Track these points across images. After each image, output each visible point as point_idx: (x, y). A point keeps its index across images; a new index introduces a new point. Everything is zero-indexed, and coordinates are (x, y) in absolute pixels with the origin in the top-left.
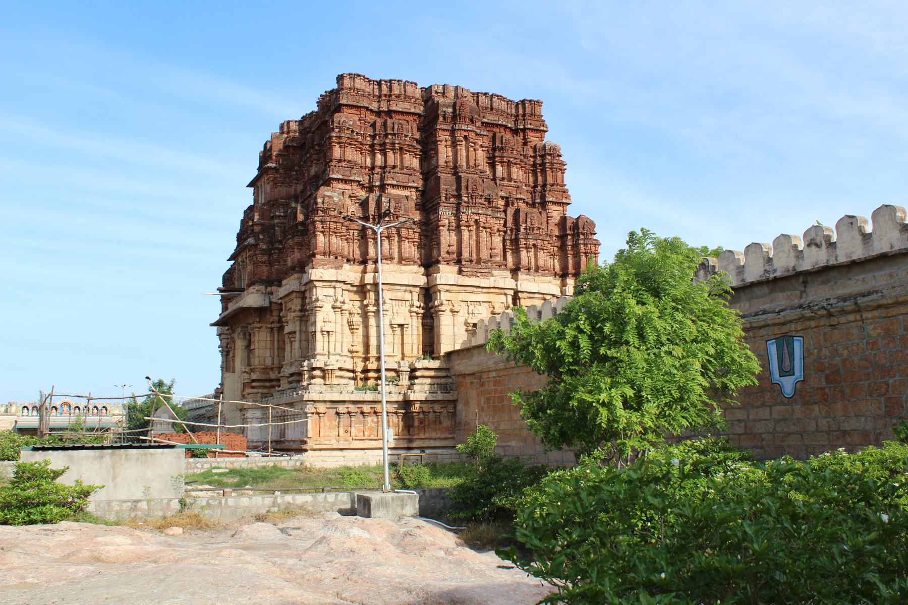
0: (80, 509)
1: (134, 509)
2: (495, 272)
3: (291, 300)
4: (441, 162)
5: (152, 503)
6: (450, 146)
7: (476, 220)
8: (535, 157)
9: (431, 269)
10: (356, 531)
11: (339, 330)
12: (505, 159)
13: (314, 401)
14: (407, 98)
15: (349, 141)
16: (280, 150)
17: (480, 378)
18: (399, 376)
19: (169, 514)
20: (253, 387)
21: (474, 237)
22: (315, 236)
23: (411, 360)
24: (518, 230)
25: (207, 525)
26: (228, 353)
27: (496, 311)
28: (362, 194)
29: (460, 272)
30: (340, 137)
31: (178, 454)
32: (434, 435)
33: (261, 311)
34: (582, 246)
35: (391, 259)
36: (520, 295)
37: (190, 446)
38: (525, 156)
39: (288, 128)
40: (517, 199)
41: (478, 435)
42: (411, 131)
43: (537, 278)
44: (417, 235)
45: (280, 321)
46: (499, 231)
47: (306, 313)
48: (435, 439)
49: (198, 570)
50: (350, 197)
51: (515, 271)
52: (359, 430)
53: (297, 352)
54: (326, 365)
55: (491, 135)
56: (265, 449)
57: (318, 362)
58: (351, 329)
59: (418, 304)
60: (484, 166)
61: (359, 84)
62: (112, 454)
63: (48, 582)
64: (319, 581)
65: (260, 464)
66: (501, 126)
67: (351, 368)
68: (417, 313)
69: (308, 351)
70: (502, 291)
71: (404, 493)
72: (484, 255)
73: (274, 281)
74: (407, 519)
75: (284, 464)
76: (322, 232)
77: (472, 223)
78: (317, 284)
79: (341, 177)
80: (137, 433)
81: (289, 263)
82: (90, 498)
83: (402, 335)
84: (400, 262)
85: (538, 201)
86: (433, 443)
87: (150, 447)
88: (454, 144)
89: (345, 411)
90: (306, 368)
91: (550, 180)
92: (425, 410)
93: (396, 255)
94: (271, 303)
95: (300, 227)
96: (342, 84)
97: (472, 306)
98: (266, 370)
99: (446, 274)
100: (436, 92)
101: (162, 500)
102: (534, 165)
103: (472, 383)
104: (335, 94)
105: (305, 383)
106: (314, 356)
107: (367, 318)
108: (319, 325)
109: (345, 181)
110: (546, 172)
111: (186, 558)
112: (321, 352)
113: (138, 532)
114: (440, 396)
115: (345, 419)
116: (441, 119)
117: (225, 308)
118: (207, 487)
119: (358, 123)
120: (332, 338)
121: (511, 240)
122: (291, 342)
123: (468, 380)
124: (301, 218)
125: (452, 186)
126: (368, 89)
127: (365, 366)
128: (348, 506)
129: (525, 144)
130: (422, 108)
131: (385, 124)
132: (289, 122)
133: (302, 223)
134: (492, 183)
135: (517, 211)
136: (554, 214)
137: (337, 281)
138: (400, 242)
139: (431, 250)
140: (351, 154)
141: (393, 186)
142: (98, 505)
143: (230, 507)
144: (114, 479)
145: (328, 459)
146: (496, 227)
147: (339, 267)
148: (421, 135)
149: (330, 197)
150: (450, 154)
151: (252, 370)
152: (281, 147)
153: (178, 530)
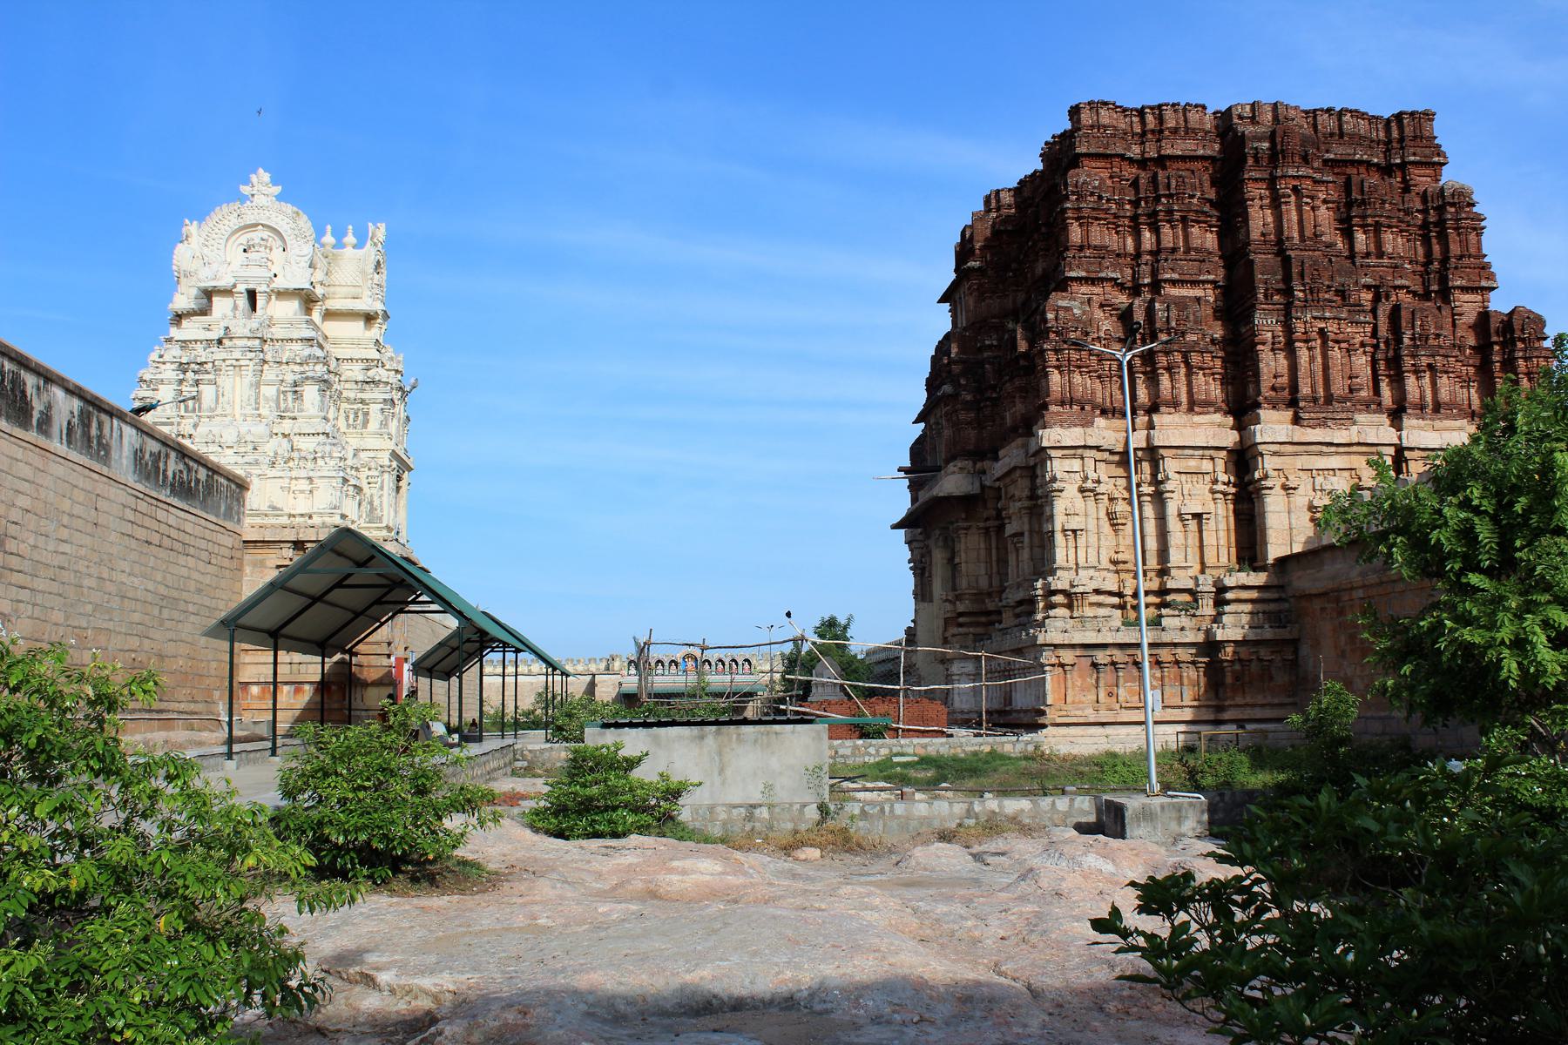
0: (668, 818)
1: (750, 817)
2: (1360, 417)
3: (1014, 482)
4: (1255, 235)
5: (777, 810)
6: (1270, 207)
7: (1321, 330)
8: (1425, 212)
9: (1246, 418)
10: (1092, 861)
11: (1092, 525)
12: (1369, 220)
13: (1056, 646)
14: (1189, 132)
15: (1094, 214)
16: (986, 239)
17: (1338, 600)
18: (1196, 601)
19: (803, 827)
20: (961, 625)
21: (1319, 359)
22: (1046, 375)
23: (1216, 573)
24: (1399, 341)
25: (859, 845)
26: (922, 574)
27: (1363, 484)
28: (1122, 299)
29: (1296, 420)
30: (1079, 209)
31: (818, 733)
32: (1260, 699)
33: (967, 503)
34: (1521, 362)
35: (1175, 404)
36: (1407, 454)
37: (856, 720)
38: (1407, 212)
39: (998, 201)
40: (1395, 287)
41: (1325, 700)
42: (1200, 189)
43: (1438, 424)
44: (1218, 363)
45: (999, 516)
46: (1363, 345)
47: (1039, 502)
48: (1263, 706)
49: (774, 917)
50: (1102, 306)
51: (1396, 416)
52: (1130, 692)
53: (1026, 567)
54: (1072, 586)
55: (1341, 180)
56: (979, 725)
57: (1060, 581)
58: (1113, 525)
59: (1225, 478)
60: (1330, 234)
61: (1105, 117)
62: (718, 733)
63: (566, 926)
64: (976, 941)
65: (968, 749)
66: (1360, 162)
67: (1115, 588)
68: (1225, 494)
69: (1044, 564)
70: (1373, 449)
71: (1185, 798)
72: (1339, 387)
73: (985, 452)
74: (1186, 841)
75: (1008, 748)
76: (1057, 367)
77: (1314, 335)
78: (1053, 453)
79: (1083, 274)
80: (791, 701)
81: (1008, 421)
82: (681, 801)
83: (1200, 531)
84: (1190, 410)
85: (1435, 287)
86: (1258, 713)
87: (788, 722)
88: (1276, 203)
89: (1107, 660)
90: (1040, 592)
91: (1455, 249)
92: (1243, 656)
93: (1184, 398)
94: (983, 487)
95: (1022, 362)
96: (1079, 120)
97: (1315, 476)
98: (979, 596)
99: (1272, 426)
100: (1240, 117)
101: (791, 805)
102: (1425, 225)
103: (1323, 609)
104: (1066, 139)
105: (1039, 617)
106: (1053, 572)
107: (1144, 510)
108: (1059, 521)
109: (1092, 281)
110: (1446, 236)
111: (781, 897)
112: (1065, 564)
113: (738, 855)
114: (1268, 633)
115: (1107, 676)
116: (1250, 161)
117: (914, 500)
118: (882, 784)
119: (1109, 182)
120: (1081, 541)
121: (1387, 360)
122: (1017, 550)
123: (1317, 605)
124: (1022, 346)
125: (1275, 274)
126: (1122, 124)
127: (1163, 584)
128: (1092, 818)
129: (1406, 188)
130: (1217, 147)
131: (1154, 180)
132: (998, 192)
133: (1025, 355)
134: (1348, 263)
135: (1396, 309)
136: (1466, 308)
137: (1085, 447)
138: (1189, 375)
139: (1245, 386)
140: (1100, 235)
141: (1174, 283)
142: (695, 810)
143: (898, 817)
144: (721, 771)
145: (1081, 740)
146: (1358, 339)
147: (1088, 423)
148: (1217, 193)
149: (1067, 309)
150: (1270, 219)
151: (958, 598)
152: (988, 232)
153: (815, 853)
